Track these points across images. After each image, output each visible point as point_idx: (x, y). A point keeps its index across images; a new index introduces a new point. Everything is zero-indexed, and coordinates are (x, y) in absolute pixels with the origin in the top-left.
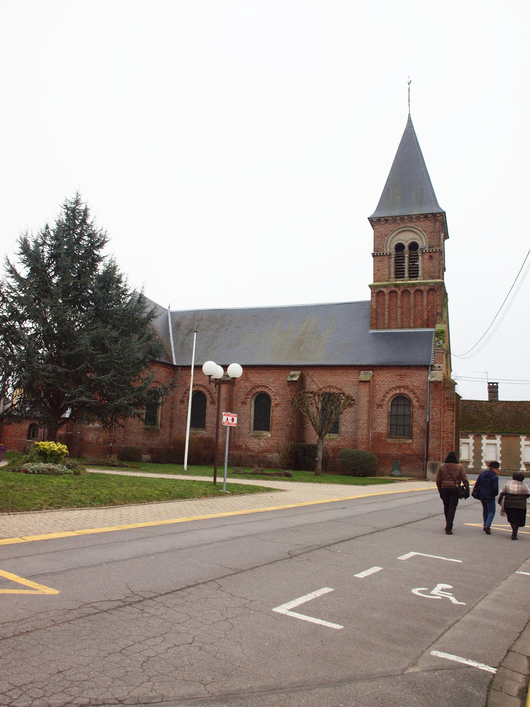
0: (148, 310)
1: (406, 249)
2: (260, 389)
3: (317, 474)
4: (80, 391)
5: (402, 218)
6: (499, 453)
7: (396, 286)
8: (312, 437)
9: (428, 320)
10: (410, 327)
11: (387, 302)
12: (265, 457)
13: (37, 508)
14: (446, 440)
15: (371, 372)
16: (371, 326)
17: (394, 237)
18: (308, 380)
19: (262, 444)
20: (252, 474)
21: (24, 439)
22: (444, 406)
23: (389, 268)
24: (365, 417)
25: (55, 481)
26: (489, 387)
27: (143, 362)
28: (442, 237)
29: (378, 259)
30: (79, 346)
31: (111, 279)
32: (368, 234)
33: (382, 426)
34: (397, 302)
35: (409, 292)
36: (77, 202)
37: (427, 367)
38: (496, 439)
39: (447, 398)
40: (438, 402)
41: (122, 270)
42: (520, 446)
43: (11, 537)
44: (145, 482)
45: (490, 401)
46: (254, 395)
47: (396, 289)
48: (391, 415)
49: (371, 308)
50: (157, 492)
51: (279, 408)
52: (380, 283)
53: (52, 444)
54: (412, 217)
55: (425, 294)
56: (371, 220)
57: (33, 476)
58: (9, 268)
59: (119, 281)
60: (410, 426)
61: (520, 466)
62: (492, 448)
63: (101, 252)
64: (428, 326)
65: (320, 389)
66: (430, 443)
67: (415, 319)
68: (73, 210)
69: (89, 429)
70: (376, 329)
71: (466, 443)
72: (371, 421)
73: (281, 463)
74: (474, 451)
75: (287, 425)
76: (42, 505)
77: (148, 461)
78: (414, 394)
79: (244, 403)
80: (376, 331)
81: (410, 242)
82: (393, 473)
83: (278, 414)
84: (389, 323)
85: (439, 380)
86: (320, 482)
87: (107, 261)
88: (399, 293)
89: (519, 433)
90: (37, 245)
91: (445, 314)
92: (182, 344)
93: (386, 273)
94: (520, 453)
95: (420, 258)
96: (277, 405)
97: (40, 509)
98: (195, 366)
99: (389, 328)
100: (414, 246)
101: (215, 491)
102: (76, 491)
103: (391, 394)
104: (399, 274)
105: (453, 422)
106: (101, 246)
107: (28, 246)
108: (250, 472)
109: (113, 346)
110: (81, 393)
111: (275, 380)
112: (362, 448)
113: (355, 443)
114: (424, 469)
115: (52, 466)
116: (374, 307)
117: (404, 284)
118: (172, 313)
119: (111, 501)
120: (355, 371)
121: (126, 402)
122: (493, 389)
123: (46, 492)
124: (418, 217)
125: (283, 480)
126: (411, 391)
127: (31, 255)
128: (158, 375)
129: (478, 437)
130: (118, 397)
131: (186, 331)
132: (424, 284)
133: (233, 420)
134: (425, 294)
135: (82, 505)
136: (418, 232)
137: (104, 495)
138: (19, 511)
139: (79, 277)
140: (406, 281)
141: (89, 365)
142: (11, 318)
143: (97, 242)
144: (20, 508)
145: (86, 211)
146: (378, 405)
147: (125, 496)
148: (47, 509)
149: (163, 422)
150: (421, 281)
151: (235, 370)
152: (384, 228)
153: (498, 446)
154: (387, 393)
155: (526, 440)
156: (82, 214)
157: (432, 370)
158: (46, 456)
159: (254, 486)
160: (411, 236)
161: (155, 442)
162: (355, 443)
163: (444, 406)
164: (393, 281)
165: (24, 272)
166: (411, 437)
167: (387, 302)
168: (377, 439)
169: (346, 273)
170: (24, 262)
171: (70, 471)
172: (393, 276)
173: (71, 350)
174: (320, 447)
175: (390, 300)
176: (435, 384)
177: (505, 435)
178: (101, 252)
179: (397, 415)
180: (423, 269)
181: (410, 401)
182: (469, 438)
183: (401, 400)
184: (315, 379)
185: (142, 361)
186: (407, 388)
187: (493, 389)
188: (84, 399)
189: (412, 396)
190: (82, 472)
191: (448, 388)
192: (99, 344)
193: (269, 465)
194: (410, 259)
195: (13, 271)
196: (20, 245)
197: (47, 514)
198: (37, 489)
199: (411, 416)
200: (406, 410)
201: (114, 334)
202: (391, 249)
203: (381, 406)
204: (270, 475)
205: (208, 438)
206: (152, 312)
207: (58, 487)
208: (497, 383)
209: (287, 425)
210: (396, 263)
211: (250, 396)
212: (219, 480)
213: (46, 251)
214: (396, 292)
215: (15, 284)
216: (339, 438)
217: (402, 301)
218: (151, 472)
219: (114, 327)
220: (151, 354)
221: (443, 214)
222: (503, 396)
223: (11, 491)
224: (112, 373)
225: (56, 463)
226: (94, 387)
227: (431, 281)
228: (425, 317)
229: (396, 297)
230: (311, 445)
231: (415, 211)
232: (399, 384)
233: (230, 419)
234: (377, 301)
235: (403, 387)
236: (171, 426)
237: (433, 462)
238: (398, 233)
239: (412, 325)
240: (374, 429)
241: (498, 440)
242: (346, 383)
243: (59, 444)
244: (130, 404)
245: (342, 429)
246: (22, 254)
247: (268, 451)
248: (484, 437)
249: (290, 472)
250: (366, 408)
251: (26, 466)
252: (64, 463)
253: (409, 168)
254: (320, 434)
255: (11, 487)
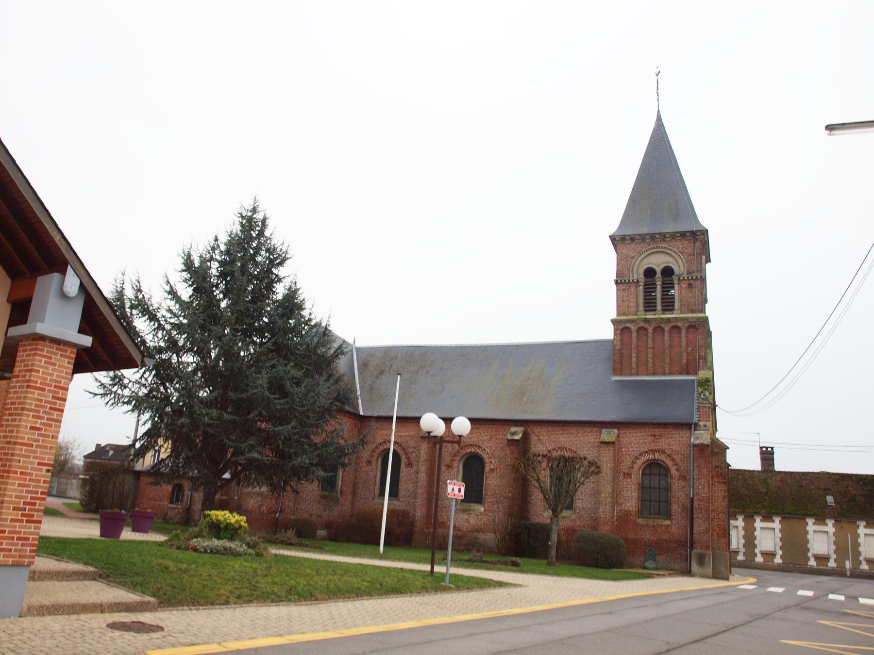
0: (336, 345)
1: (658, 275)
2: (471, 450)
3: (550, 564)
4: (251, 445)
5: (653, 237)
6: (778, 540)
7: (646, 321)
8: (541, 514)
9: (688, 364)
10: (664, 374)
11: (634, 341)
12: (476, 538)
13: (222, 602)
14: (716, 522)
15: (616, 431)
16: (614, 371)
17: (642, 260)
18: (534, 439)
19: (472, 521)
20: (468, 561)
21: (166, 503)
22: (712, 478)
23: (637, 298)
24: (609, 489)
25: (237, 564)
26: (762, 453)
27: (328, 410)
28: (704, 261)
29: (623, 287)
30: (256, 387)
31: (291, 304)
32: (610, 256)
33: (631, 501)
34: (647, 341)
35: (663, 329)
36: (254, 210)
37: (689, 426)
38: (774, 521)
39: (716, 467)
40: (705, 471)
41: (305, 294)
42: (807, 533)
43: (206, 643)
44: (347, 569)
45: (764, 471)
46: (463, 456)
47: (647, 326)
48: (642, 487)
49: (614, 347)
50: (366, 584)
51: (494, 474)
52: (625, 318)
53: (227, 513)
54: (665, 236)
55: (684, 332)
56: (613, 238)
57: (206, 556)
58: (119, 289)
59: (300, 307)
60: (668, 503)
61: (808, 559)
62: (769, 534)
63: (281, 271)
64: (688, 373)
65: (549, 452)
66: (695, 527)
67: (670, 364)
68: (250, 220)
69: (249, 493)
70: (621, 375)
71: (823, 532)
72: (616, 494)
73: (498, 547)
74: (744, 537)
75: (505, 498)
76: (228, 597)
77: (323, 539)
78: (673, 460)
79: (369, 462)
80: (619, 378)
81: (663, 266)
82: (647, 564)
83: (494, 481)
84: (637, 367)
85: (706, 443)
86: (558, 575)
87: (287, 283)
88: (650, 330)
89: (803, 514)
90: (203, 261)
91: (709, 358)
92: (371, 388)
93: (633, 304)
94: (808, 541)
95: (676, 286)
96: (492, 470)
97: (227, 603)
98: (397, 418)
99: (637, 374)
100: (668, 272)
101: (435, 584)
102: (266, 579)
103: (642, 460)
104: (650, 305)
105: (725, 498)
106: (281, 263)
107: (192, 263)
108: (466, 557)
109: (296, 389)
110: (252, 448)
111: (491, 438)
112: (604, 530)
113: (595, 523)
114: (688, 560)
115: (229, 544)
116: (618, 347)
117: (656, 319)
118: (358, 349)
119: (312, 595)
120: (595, 429)
121: (308, 462)
122: (767, 455)
123: (229, 580)
124: (673, 236)
125: (510, 571)
126: (669, 456)
127: (196, 273)
128: (341, 428)
129: (749, 518)
130: (297, 454)
131: (375, 373)
132: (682, 319)
133: (459, 490)
134: (684, 332)
135: (277, 599)
136: (673, 254)
137: (302, 586)
138: (202, 605)
139: (253, 301)
140: (659, 315)
141: (264, 412)
142: (167, 349)
143: (277, 258)
144: (202, 601)
145: (264, 221)
146: (625, 474)
147: (328, 588)
148: (235, 603)
149: (344, 488)
150: (678, 316)
151: (462, 425)
152: (629, 249)
153: (777, 531)
154: (637, 458)
155: (814, 524)
156: (260, 224)
157: (695, 430)
158: (218, 530)
159: (481, 579)
160: (663, 258)
161: (335, 513)
162: (595, 523)
163: (712, 478)
164: (642, 315)
165: (186, 292)
166: (668, 516)
167: (634, 341)
168: (624, 518)
169: (583, 306)
170: (185, 281)
171: (250, 551)
172: (641, 308)
173: (242, 393)
174: (555, 528)
175: (638, 339)
176: (701, 448)
177: (785, 517)
178: (281, 271)
179: (650, 488)
180: (681, 301)
181: (667, 470)
182: (737, 519)
183: (655, 468)
184: (542, 438)
185: (326, 410)
186: (663, 452)
187: (767, 455)
188: (256, 455)
189: (669, 463)
190: (265, 553)
191: (717, 454)
192: (277, 387)
193: (482, 548)
194: (663, 288)
195: (173, 293)
196: (182, 261)
197: (237, 610)
198: (216, 575)
199: (668, 489)
200: (662, 482)
201: (298, 374)
202: (638, 275)
203: (629, 475)
204: (491, 563)
205: (403, 511)
206: (340, 347)
207: (242, 572)
208: (772, 448)
209: (505, 498)
210: (645, 292)
211: (457, 458)
212: (437, 569)
213: (214, 268)
214: (646, 329)
215: (175, 308)
216: (574, 516)
217: (653, 340)
218: (339, 555)
219: (296, 365)
220: (339, 401)
221: (705, 232)
222: (780, 465)
223: (186, 576)
224: (293, 423)
225: (231, 539)
226: (267, 440)
227: (691, 315)
228: (685, 361)
229: (646, 335)
230: (538, 524)
231: (669, 228)
232: (652, 447)
233: (456, 489)
234: (621, 340)
235: (658, 451)
236: (354, 493)
237: (700, 551)
238: (645, 257)
239: (667, 371)
240: (620, 505)
241: (776, 524)
242: (582, 445)
243: (235, 514)
244: (311, 464)
245: (578, 504)
246: (183, 271)
247: (480, 530)
248: (758, 519)
249: (518, 560)
250: (609, 478)
251: (194, 542)
252: (242, 540)
253: (659, 173)
254: (555, 512)
255: (185, 571)
